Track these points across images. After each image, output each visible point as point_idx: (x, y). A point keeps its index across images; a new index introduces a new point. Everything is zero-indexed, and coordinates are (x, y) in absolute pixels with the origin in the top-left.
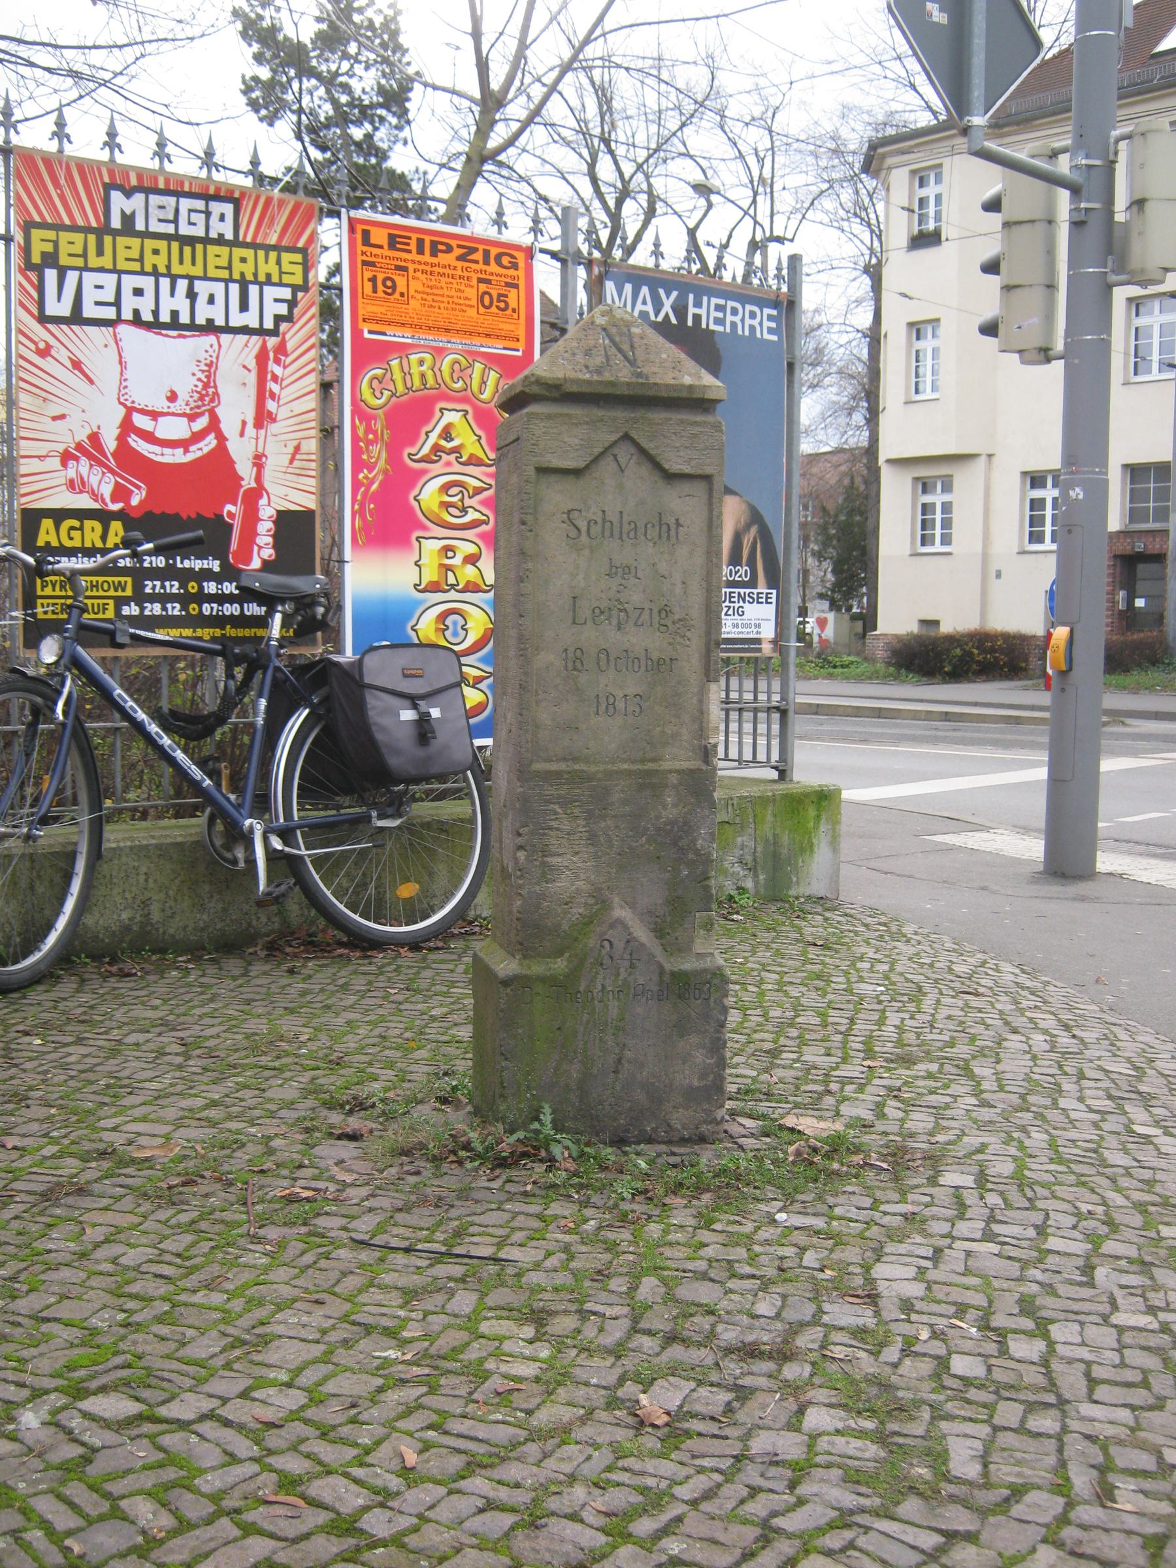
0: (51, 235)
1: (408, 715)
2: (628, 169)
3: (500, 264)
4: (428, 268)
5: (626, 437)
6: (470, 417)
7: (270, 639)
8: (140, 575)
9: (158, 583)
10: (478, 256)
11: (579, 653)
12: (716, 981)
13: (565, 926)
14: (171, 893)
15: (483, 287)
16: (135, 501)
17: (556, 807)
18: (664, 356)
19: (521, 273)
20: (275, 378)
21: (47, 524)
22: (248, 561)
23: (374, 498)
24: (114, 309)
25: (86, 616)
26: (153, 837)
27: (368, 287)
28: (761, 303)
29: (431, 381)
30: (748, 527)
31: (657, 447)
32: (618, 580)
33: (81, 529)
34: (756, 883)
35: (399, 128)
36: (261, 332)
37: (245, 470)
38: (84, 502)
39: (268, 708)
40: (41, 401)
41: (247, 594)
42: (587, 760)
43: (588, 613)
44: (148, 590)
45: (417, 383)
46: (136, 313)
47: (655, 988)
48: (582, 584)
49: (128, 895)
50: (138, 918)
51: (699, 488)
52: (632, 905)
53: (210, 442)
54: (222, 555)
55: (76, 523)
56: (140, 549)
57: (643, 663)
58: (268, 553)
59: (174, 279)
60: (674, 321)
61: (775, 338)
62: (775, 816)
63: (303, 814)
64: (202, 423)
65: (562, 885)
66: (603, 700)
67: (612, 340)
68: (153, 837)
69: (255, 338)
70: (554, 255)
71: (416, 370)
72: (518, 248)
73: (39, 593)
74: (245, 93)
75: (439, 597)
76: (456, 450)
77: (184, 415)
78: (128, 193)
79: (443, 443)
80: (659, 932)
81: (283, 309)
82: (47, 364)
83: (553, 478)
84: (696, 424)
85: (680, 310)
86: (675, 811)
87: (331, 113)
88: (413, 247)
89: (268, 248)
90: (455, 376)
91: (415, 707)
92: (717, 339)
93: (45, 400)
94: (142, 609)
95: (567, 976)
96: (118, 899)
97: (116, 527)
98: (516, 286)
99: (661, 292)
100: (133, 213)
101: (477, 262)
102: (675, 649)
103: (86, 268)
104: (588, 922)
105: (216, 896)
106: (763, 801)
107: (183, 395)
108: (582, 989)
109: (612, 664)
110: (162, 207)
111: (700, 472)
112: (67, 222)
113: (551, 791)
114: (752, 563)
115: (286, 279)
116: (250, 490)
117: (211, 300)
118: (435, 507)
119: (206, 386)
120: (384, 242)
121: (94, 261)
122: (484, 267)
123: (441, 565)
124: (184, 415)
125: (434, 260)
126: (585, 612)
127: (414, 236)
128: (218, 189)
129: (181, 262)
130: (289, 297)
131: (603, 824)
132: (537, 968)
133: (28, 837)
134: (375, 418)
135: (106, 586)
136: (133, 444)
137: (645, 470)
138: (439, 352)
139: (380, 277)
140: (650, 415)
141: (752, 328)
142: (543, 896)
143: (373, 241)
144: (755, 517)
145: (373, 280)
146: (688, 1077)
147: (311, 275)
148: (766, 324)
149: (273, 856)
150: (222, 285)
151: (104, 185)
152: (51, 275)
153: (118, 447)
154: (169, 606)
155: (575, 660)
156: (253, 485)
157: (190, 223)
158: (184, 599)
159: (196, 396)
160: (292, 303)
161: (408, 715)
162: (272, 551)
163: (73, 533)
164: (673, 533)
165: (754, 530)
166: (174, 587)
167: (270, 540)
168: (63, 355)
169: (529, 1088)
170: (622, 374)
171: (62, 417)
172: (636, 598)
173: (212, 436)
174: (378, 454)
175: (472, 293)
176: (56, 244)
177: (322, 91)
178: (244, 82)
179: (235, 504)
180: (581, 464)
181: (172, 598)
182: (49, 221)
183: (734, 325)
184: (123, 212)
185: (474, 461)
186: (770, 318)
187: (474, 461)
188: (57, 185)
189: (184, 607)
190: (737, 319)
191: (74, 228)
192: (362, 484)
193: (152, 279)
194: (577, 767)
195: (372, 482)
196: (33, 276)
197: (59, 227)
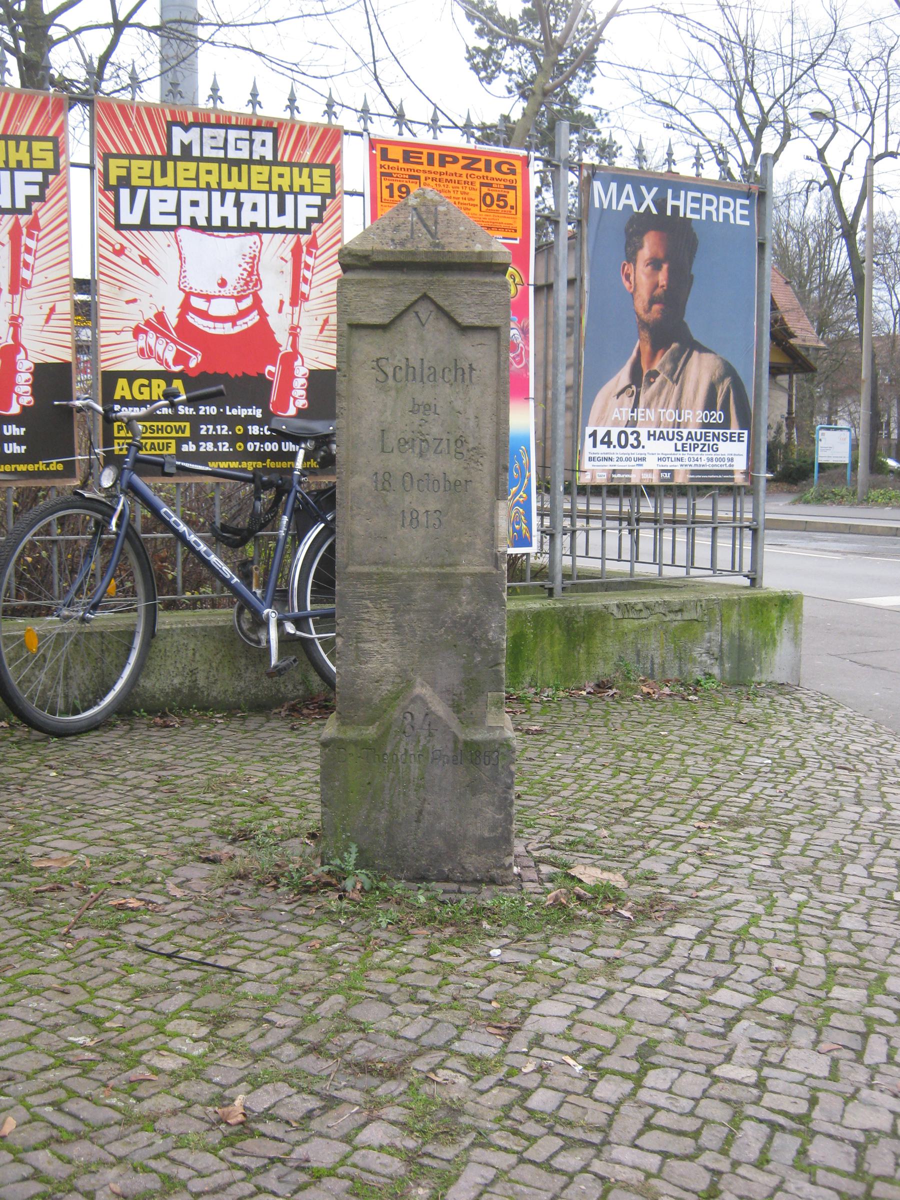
0: (125, 163)
2: (767, 103)
4: (438, 176)
5: (425, 297)
7: (295, 469)
8: (196, 421)
9: (211, 427)
10: (481, 165)
11: (387, 476)
12: (503, 750)
13: (376, 700)
14: (214, 665)
15: (485, 190)
16: (192, 364)
17: (368, 602)
18: (462, 229)
19: (519, 177)
20: (307, 267)
21: (122, 382)
22: (286, 409)
24: (175, 217)
25: (144, 452)
26: (200, 622)
27: (386, 193)
28: (735, 195)
30: (721, 379)
31: (451, 305)
32: (421, 415)
33: (150, 386)
34: (722, 671)
35: (586, 80)
36: (296, 231)
37: (283, 339)
38: (152, 365)
39: (289, 523)
41: (280, 436)
42: (395, 564)
43: (395, 443)
44: (203, 432)
46: (193, 219)
47: (450, 754)
48: (390, 419)
49: (179, 665)
50: (188, 684)
51: (488, 339)
52: (433, 684)
53: (253, 318)
54: (263, 403)
55: (146, 382)
56: (176, 400)
57: (442, 483)
58: (302, 403)
59: (224, 193)
60: (654, 212)
61: (747, 223)
62: (740, 616)
63: (316, 606)
64: (247, 303)
65: (373, 666)
66: (408, 515)
67: (420, 218)
68: (200, 622)
69: (291, 236)
73: (116, 434)
74: (468, 60)
77: (232, 297)
78: (186, 128)
80: (457, 708)
81: (314, 213)
82: (121, 261)
83: (363, 332)
84: (486, 284)
85: (660, 203)
86: (469, 607)
87: (535, 71)
88: (424, 160)
89: (301, 166)
92: (693, 225)
93: (120, 288)
94: (198, 447)
95: (376, 741)
96: (171, 668)
98: (514, 188)
99: (643, 188)
100: (191, 143)
101: (480, 170)
102: (469, 473)
103: (153, 187)
104: (396, 697)
105: (251, 668)
106: (730, 603)
107: (231, 282)
108: (388, 752)
109: (415, 485)
110: (214, 138)
111: (488, 324)
112: (138, 152)
113: (363, 589)
114: (725, 408)
115: (316, 189)
117: (254, 208)
119: (250, 274)
120: (400, 157)
121: (159, 181)
124: (232, 297)
125: (443, 170)
126: (392, 440)
127: (425, 151)
128: (259, 122)
129: (230, 179)
130: (319, 203)
131: (407, 617)
132: (351, 734)
133: (83, 620)
135: (169, 429)
136: (191, 321)
137: (443, 324)
139: (396, 185)
140: (445, 278)
141: (726, 216)
142: (356, 675)
143: (390, 156)
144: (729, 371)
145: (390, 187)
146: (480, 829)
147: (338, 185)
148: (739, 212)
149: (285, 640)
150: (264, 195)
151: (167, 122)
152: (125, 193)
154: (220, 444)
156: (290, 350)
157: (237, 149)
158: (232, 439)
159: (242, 282)
162: (305, 401)
163: (143, 389)
164: (467, 376)
165: (727, 381)
166: (224, 430)
167: (304, 393)
168: (134, 254)
169: (344, 830)
170: (423, 245)
171: (135, 301)
173: (256, 312)
175: (475, 195)
176: (129, 169)
177: (527, 56)
178: (468, 51)
179: (275, 365)
180: (386, 320)
181: (222, 438)
183: (709, 213)
184: (182, 142)
186: (743, 207)
188: (129, 124)
189: (232, 445)
190: (712, 209)
191: (144, 157)
193: (206, 193)
194: (385, 570)
196: (111, 195)
197: (132, 157)
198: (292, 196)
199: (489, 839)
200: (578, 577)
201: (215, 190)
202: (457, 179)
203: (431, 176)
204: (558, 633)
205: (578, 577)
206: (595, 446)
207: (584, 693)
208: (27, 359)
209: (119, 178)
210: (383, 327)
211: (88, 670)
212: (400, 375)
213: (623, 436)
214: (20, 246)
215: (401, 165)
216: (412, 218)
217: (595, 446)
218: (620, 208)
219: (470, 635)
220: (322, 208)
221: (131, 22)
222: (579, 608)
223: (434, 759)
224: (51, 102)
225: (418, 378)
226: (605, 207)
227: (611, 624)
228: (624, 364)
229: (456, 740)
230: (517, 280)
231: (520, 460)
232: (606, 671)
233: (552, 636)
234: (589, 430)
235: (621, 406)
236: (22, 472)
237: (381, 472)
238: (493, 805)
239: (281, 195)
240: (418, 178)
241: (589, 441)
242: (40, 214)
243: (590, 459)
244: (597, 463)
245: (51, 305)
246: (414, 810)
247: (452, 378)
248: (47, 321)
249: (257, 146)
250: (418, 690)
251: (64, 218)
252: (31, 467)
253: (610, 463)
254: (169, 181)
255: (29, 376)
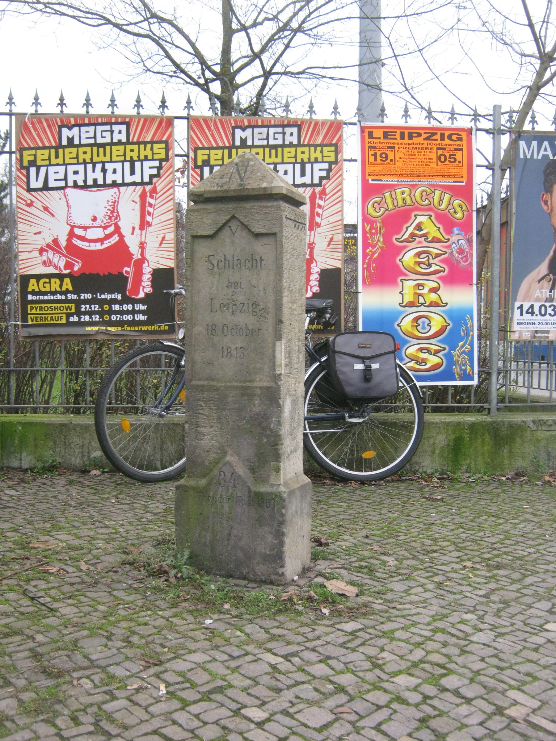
0: (207, 152)
1: (359, 367)
3: (451, 140)
4: (407, 146)
5: (233, 217)
6: (433, 218)
9: (88, 306)
10: (438, 137)
11: (214, 326)
12: (277, 499)
15: (440, 152)
16: (76, 268)
17: (202, 403)
18: (259, 174)
19: (464, 142)
21: (33, 281)
23: (375, 261)
27: (372, 159)
29: (408, 201)
32: (232, 289)
33: (50, 282)
36: (142, 183)
37: (135, 250)
38: (51, 270)
40: (28, 227)
43: (218, 307)
44: (83, 309)
45: (400, 203)
46: (75, 182)
47: (247, 499)
48: (215, 292)
52: (239, 455)
54: (122, 290)
55: (47, 280)
64: (112, 229)
65: (205, 442)
66: (225, 350)
67: (238, 170)
70: (487, 131)
71: (400, 197)
72: (463, 130)
73: (29, 312)
75: (415, 309)
76: (425, 235)
77: (101, 227)
78: (70, 128)
79: (417, 232)
80: (253, 470)
82: (32, 210)
83: (201, 240)
84: (268, 207)
86: (259, 408)
88: (398, 136)
89: (316, 146)
90: (423, 198)
91: (363, 363)
94: (80, 318)
97: (67, 281)
98: (462, 150)
101: (437, 140)
102: (260, 324)
103: (50, 165)
107: (100, 217)
111: (270, 232)
112: (215, 145)
116: (137, 261)
118: (412, 265)
119: (112, 212)
122: (441, 142)
123: (415, 293)
124: (101, 227)
125: (411, 142)
126: (216, 306)
128: (289, 122)
129: (98, 155)
131: (224, 413)
134: (376, 222)
135: (62, 308)
136: (75, 242)
137: (245, 233)
138: (414, 187)
139: (379, 153)
140: (245, 205)
145: (375, 155)
146: (264, 548)
147: (339, 156)
150: (121, 164)
152: (33, 170)
153: (67, 244)
154: (93, 316)
155: (212, 330)
156: (140, 257)
158: (101, 314)
159: (107, 217)
160: (159, 168)
161: (359, 367)
162: (318, 288)
163: (45, 285)
164: (259, 264)
166: (96, 308)
169: (187, 541)
171: (39, 233)
172: (241, 298)
173: (117, 235)
174: (378, 240)
175: (434, 156)
179: (129, 267)
181: (95, 313)
182: (32, 146)
185: (435, 240)
187: (435, 240)
188: (209, 129)
192: (368, 255)
194: (212, 383)
195: (374, 253)
197: (211, 148)
198: (310, 165)
199: (269, 555)
200: (532, 402)
201: (89, 163)
202: (420, 147)
203: (402, 146)
204: (487, 438)
205: (532, 402)
206: (522, 314)
207: (504, 478)
208: (149, 266)
209: (203, 161)
210: (211, 237)
211: (174, 446)
212: (221, 264)
213: (543, 308)
214: (146, 203)
215: (382, 140)
216: (233, 170)
217: (522, 314)
218: (540, 157)
219: (260, 426)
220: (329, 171)
221: (273, 71)
222: (503, 422)
223: (237, 502)
224: (164, 121)
225: (231, 266)
226: (528, 157)
227: (528, 434)
228: (543, 261)
229: (250, 491)
230: (464, 208)
231: (466, 324)
232: (524, 465)
233: (483, 439)
234: (517, 304)
235: (542, 288)
236: (145, 331)
237: (210, 324)
238: (272, 534)
239: (303, 164)
240: (394, 148)
241: (517, 312)
242: (157, 185)
243: (518, 324)
244: (523, 326)
245: (163, 235)
246: (226, 533)
247: (250, 266)
248: (161, 245)
249: (287, 137)
250: (228, 458)
251: (339, 188)
252: (150, 328)
253: (533, 326)
254: (60, 160)
255: (150, 276)
